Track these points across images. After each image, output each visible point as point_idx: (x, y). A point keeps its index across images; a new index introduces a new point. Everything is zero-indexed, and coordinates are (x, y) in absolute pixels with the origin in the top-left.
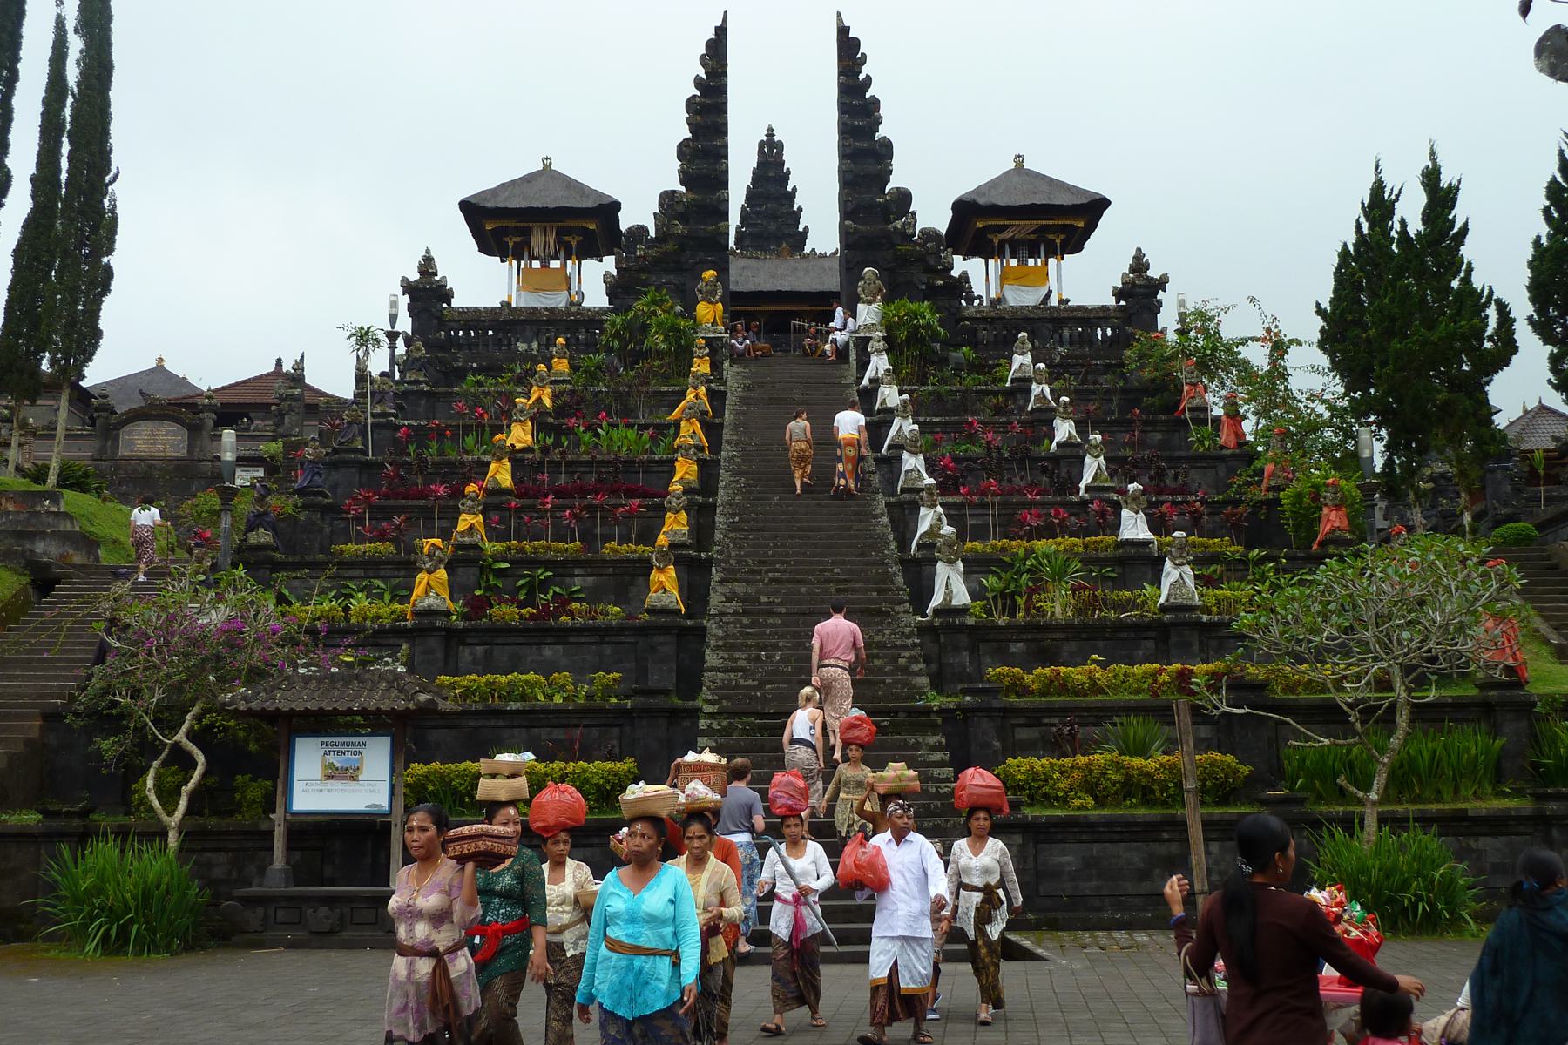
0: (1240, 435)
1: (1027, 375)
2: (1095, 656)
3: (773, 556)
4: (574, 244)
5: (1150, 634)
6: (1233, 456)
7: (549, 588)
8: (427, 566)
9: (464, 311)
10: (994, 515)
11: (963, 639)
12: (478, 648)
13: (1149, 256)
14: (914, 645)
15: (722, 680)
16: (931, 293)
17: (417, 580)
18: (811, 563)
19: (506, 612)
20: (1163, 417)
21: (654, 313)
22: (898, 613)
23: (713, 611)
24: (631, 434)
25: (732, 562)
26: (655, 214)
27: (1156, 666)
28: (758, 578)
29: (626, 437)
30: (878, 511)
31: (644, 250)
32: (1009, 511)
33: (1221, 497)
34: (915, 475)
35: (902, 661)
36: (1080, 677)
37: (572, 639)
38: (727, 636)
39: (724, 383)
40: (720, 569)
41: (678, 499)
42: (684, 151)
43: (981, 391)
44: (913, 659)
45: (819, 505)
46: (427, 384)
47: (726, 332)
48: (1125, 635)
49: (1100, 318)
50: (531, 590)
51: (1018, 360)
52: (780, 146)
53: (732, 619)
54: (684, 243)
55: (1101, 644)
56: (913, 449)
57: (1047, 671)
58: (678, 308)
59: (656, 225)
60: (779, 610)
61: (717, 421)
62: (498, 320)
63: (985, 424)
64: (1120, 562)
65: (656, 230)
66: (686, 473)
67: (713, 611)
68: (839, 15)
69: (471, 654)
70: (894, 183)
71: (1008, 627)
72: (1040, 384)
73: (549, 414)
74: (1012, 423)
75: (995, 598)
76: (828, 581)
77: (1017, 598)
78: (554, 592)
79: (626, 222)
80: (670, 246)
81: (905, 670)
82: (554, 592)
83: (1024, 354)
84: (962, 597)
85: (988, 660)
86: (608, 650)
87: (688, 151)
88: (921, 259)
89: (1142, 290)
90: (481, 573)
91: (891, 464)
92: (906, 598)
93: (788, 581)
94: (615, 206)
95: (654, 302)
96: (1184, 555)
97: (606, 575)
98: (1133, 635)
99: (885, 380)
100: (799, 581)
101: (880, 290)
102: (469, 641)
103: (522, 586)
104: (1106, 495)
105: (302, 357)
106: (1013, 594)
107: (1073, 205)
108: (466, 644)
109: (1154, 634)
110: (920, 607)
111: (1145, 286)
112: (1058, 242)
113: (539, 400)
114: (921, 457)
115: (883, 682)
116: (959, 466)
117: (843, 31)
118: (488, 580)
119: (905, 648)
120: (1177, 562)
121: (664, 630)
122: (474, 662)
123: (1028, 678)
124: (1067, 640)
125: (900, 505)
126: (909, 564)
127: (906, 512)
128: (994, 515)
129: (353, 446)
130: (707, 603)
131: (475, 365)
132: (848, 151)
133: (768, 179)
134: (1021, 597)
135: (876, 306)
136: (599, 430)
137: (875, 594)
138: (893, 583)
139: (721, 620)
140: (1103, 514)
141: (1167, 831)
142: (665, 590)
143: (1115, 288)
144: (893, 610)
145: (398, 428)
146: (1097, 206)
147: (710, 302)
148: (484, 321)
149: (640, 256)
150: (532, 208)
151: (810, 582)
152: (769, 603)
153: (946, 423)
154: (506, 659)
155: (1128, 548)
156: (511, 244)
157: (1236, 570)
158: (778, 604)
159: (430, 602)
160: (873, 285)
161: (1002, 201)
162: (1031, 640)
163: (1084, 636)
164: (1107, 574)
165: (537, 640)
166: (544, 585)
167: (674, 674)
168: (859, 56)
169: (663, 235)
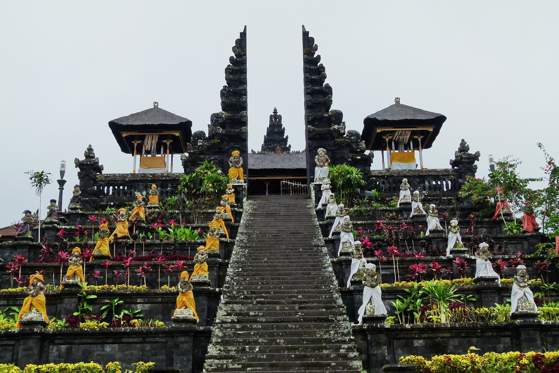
0: (535, 224)
1: (408, 201)
2: (473, 348)
3: (261, 289)
4: (168, 144)
5: (506, 333)
6: (531, 236)
7: (121, 311)
8: (31, 292)
9: (107, 176)
10: (396, 268)
11: (383, 338)
12: (62, 346)
13: (468, 143)
14: (351, 341)
15: (217, 365)
16: (354, 163)
17: (25, 301)
18: (284, 293)
19: (90, 324)
20: (487, 220)
21: (206, 173)
22: (339, 321)
23: (217, 321)
24: (188, 231)
25: (234, 292)
26: (209, 125)
27: (518, 353)
28: (250, 301)
29: (184, 233)
30: (326, 265)
31: (202, 142)
32: (405, 266)
33: (533, 255)
35: (342, 351)
36: (465, 361)
37: (124, 340)
38: (225, 336)
39: (242, 207)
40: (225, 296)
41: (202, 255)
42: (224, 93)
43: (383, 210)
44: (350, 349)
45: (291, 262)
46: (81, 210)
47: (245, 183)
49: (445, 175)
50: (110, 312)
51: (402, 193)
52: (280, 117)
53: (229, 325)
54: (222, 137)
55: (474, 340)
56: (347, 230)
57: (442, 357)
58: (220, 171)
59: (209, 130)
60: (261, 319)
61: (236, 224)
62: (125, 180)
63: (387, 224)
64: (477, 291)
65: (209, 133)
66: (212, 245)
67: (217, 321)
68: (303, 26)
69: (57, 350)
70: (333, 107)
71: (412, 329)
73: (143, 222)
74: (402, 223)
75: (401, 314)
76: (294, 303)
77: (415, 313)
78: (124, 313)
79: (194, 129)
80: (216, 141)
81: (345, 357)
82: (124, 313)
84: (381, 309)
85: (400, 351)
86: (148, 347)
87: (225, 92)
88: (349, 145)
89: (466, 160)
90: (79, 301)
91: (335, 243)
92: (344, 312)
93: (269, 303)
94: (189, 124)
95: (207, 168)
96: (526, 280)
97: (157, 303)
98: (495, 334)
99: (330, 201)
100: (275, 303)
101: (327, 160)
102: (57, 341)
103: (105, 310)
104: (463, 255)
105: (38, 211)
106: (412, 312)
107: (427, 119)
108: (54, 344)
109: (509, 333)
110: (353, 317)
111: (468, 158)
112: (420, 139)
113: (137, 214)
114: (351, 234)
115: (329, 365)
116: (374, 244)
117: (305, 34)
118: (83, 306)
119: (344, 342)
120: (522, 285)
121: (185, 333)
122: (59, 356)
123: (428, 363)
124: (452, 337)
125: (340, 263)
126: (345, 294)
127: (344, 267)
128: (396, 268)
129: (26, 236)
130: (215, 316)
131: (112, 204)
132: (309, 91)
133: (274, 133)
134: (418, 314)
136: (170, 229)
137: (324, 310)
138: (335, 303)
139: (222, 326)
140: (462, 265)
141: (58, 339)
142: (186, 307)
143: (451, 160)
144: (336, 319)
145: (58, 230)
146: (439, 121)
147: (236, 167)
148: (118, 181)
149: (200, 145)
150: (146, 124)
151: (283, 303)
152: (255, 316)
153: (365, 224)
154: (80, 354)
155: (482, 282)
156: (136, 145)
157: (551, 296)
158: (261, 316)
159: (33, 316)
160: (323, 158)
161: (390, 118)
162: (429, 338)
163: (463, 335)
165: (101, 341)
166: (118, 309)
167: (191, 363)
168: (314, 46)
169: (213, 135)
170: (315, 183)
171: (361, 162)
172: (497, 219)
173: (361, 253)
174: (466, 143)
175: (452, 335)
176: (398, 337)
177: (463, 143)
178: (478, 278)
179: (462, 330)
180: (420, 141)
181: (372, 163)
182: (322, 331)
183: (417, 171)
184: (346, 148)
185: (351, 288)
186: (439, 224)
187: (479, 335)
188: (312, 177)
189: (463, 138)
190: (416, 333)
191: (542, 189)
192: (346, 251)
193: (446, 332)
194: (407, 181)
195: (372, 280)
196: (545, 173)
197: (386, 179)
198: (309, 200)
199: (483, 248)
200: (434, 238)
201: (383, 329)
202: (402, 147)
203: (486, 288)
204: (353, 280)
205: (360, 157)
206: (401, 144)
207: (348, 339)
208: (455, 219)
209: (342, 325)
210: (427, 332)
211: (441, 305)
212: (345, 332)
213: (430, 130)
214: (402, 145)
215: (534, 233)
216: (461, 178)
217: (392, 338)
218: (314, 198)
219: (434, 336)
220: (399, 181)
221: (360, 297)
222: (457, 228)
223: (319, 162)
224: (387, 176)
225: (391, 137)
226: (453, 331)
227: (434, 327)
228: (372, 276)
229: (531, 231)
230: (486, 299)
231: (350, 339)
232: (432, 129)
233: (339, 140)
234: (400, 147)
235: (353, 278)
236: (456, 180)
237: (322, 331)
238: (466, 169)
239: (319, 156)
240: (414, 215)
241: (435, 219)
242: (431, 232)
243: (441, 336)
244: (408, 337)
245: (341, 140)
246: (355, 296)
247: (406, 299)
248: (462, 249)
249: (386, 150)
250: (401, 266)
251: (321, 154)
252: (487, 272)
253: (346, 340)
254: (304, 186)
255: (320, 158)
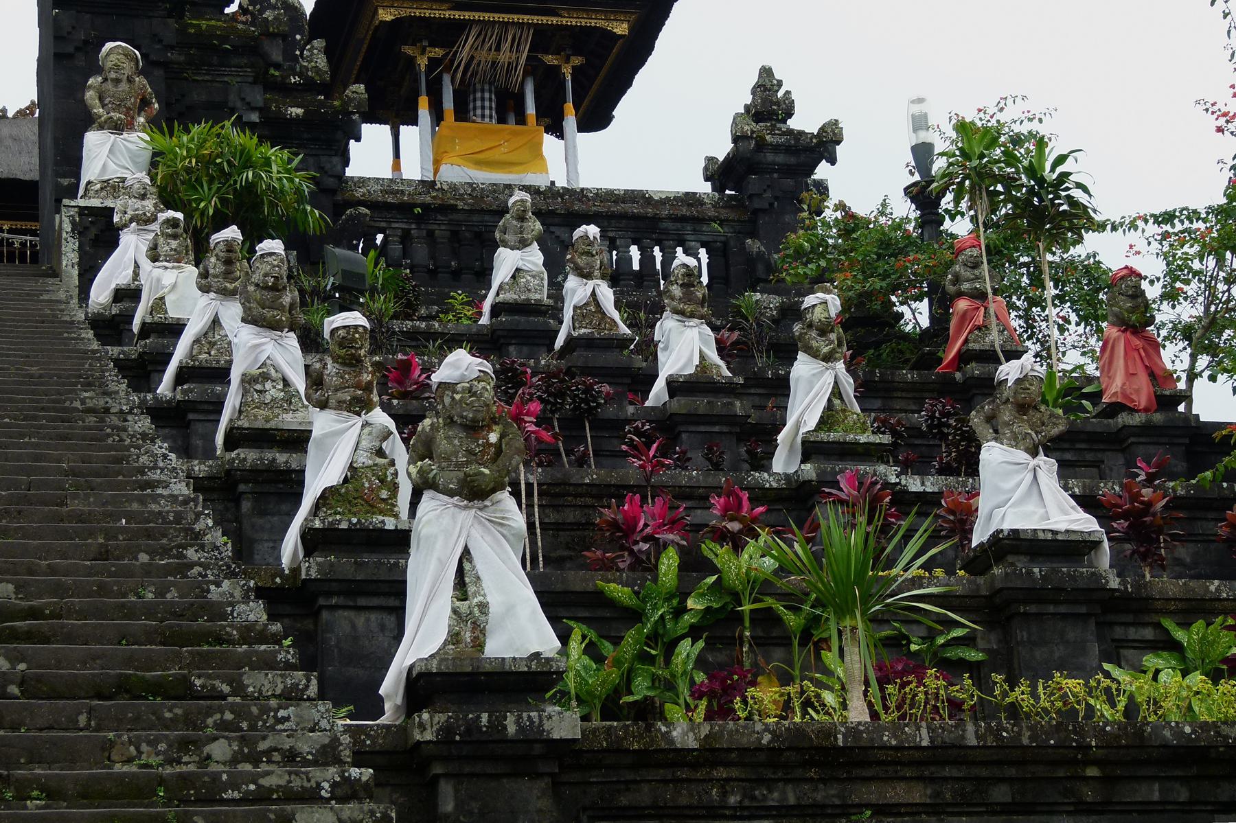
1: (534, 297)
13: (791, 82)
32: (571, 516)
34: (273, 392)
48: (1155, 793)
49: (683, 219)
51: (506, 262)
56: (268, 313)
72: (588, 276)
83: (523, 244)
89: (780, 158)
91: (187, 425)
98: (1182, 794)
111: (787, 149)
112: (567, 71)
127: (246, 506)
135: (137, 141)
143: (710, 160)
144: (238, 689)
155: (1021, 563)
160: (124, 86)
163: (1001, 794)
164: (952, 654)
170: (82, 203)
171: (305, 136)
172: (958, 375)
173: (366, 377)
174: (780, 83)
175: (937, 794)
176: (624, 801)
177: (767, 84)
178: (996, 538)
179: (999, 763)
180: (569, 78)
181: (358, 139)
182: (149, 743)
183: (562, 196)
184: (235, 61)
185: (304, 566)
186: (713, 356)
187: (1089, 795)
188: (65, 182)
189: (767, 64)
190: (727, 780)
191: (1201, 206)
192: (259, 424)
193: (904, 779)
194: (529, 204)
195: (470, 452)
196: (1220, 130)
197: (419, 219)
198: (56, 280)
199: (1018, 381)
200: (693, 418)
201: (538, 749)
202: (487, 104)
203: (1035, 594)
204: (317, 524)
205: (300, 111)
206: (483, 91)
207: (334, 785)
208: (828, 292)
209: (282, 713)
210: (799, 773)
211: (847, 634)
212: (305, 748)
213: (618, 31)
214: (487, 95)
215: (1158, 418)
216: (753, 235)
217: (585, 809)
218: (75, 272)
219: (837, 802)
220: (478, 235)
221: (354, 626)
222: (833, 336)
223: (103, 106)
224: (425, 207)
225: (437, 52)
226: (947, 771)
227: (840, 743)
228: (474, 428)
229: (1143, 404)
230: (1037, 654)
231: (347, 780)
232: (625, 25)
233: (204, 24)
234: (479, 103)
235: (315, 515)
236: (732, 243)
237: (153, 743)
238: (776, 198)
239: (105, 80)
240: (575, 334)
241: (696, 330)
242: (674, 386)
243: (873, 799)
244: (683, 801)
245: (213, 23)
246: (325, 615)
247: (616, 641)
248: (863, 439)
249: (414, 122)
250: (553, 517)
251: (117, 68)
252: (1042, 511)
253: (319, 787)
254: (23, 244)
255: (109, 86)
